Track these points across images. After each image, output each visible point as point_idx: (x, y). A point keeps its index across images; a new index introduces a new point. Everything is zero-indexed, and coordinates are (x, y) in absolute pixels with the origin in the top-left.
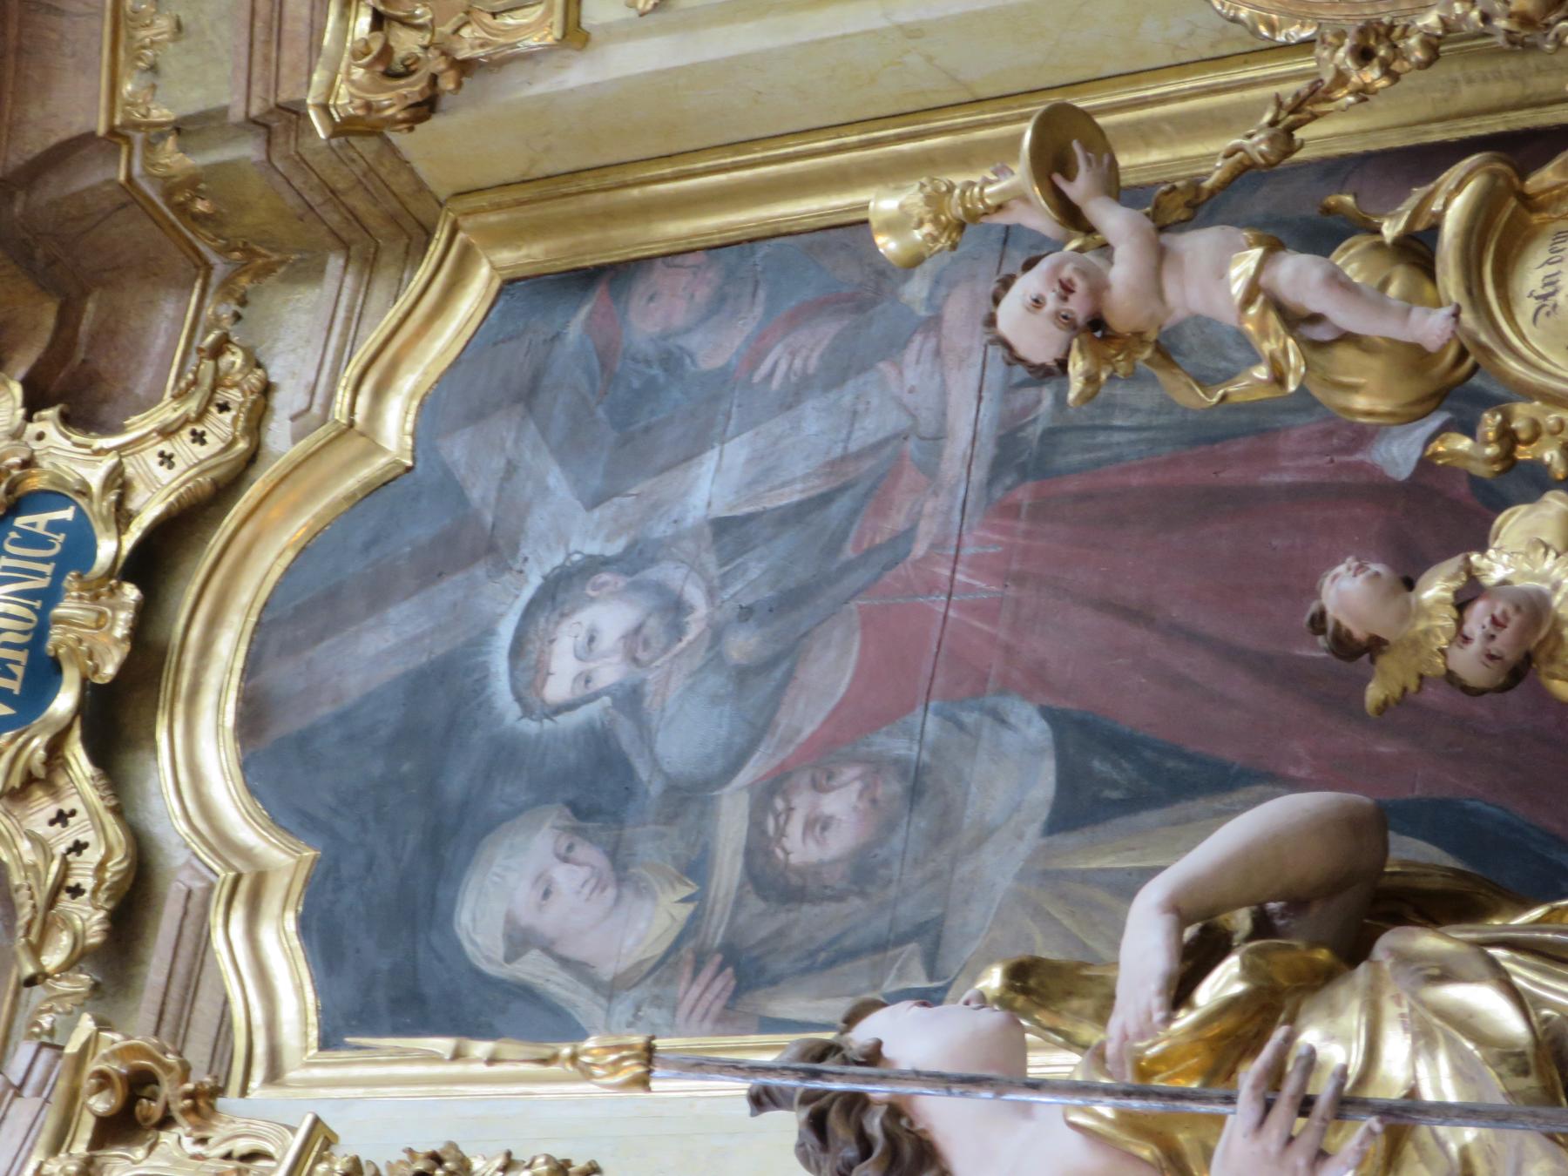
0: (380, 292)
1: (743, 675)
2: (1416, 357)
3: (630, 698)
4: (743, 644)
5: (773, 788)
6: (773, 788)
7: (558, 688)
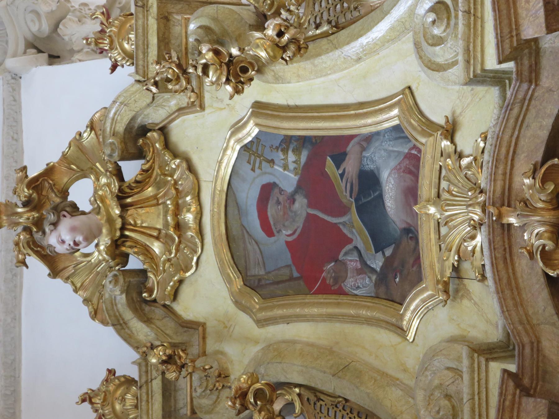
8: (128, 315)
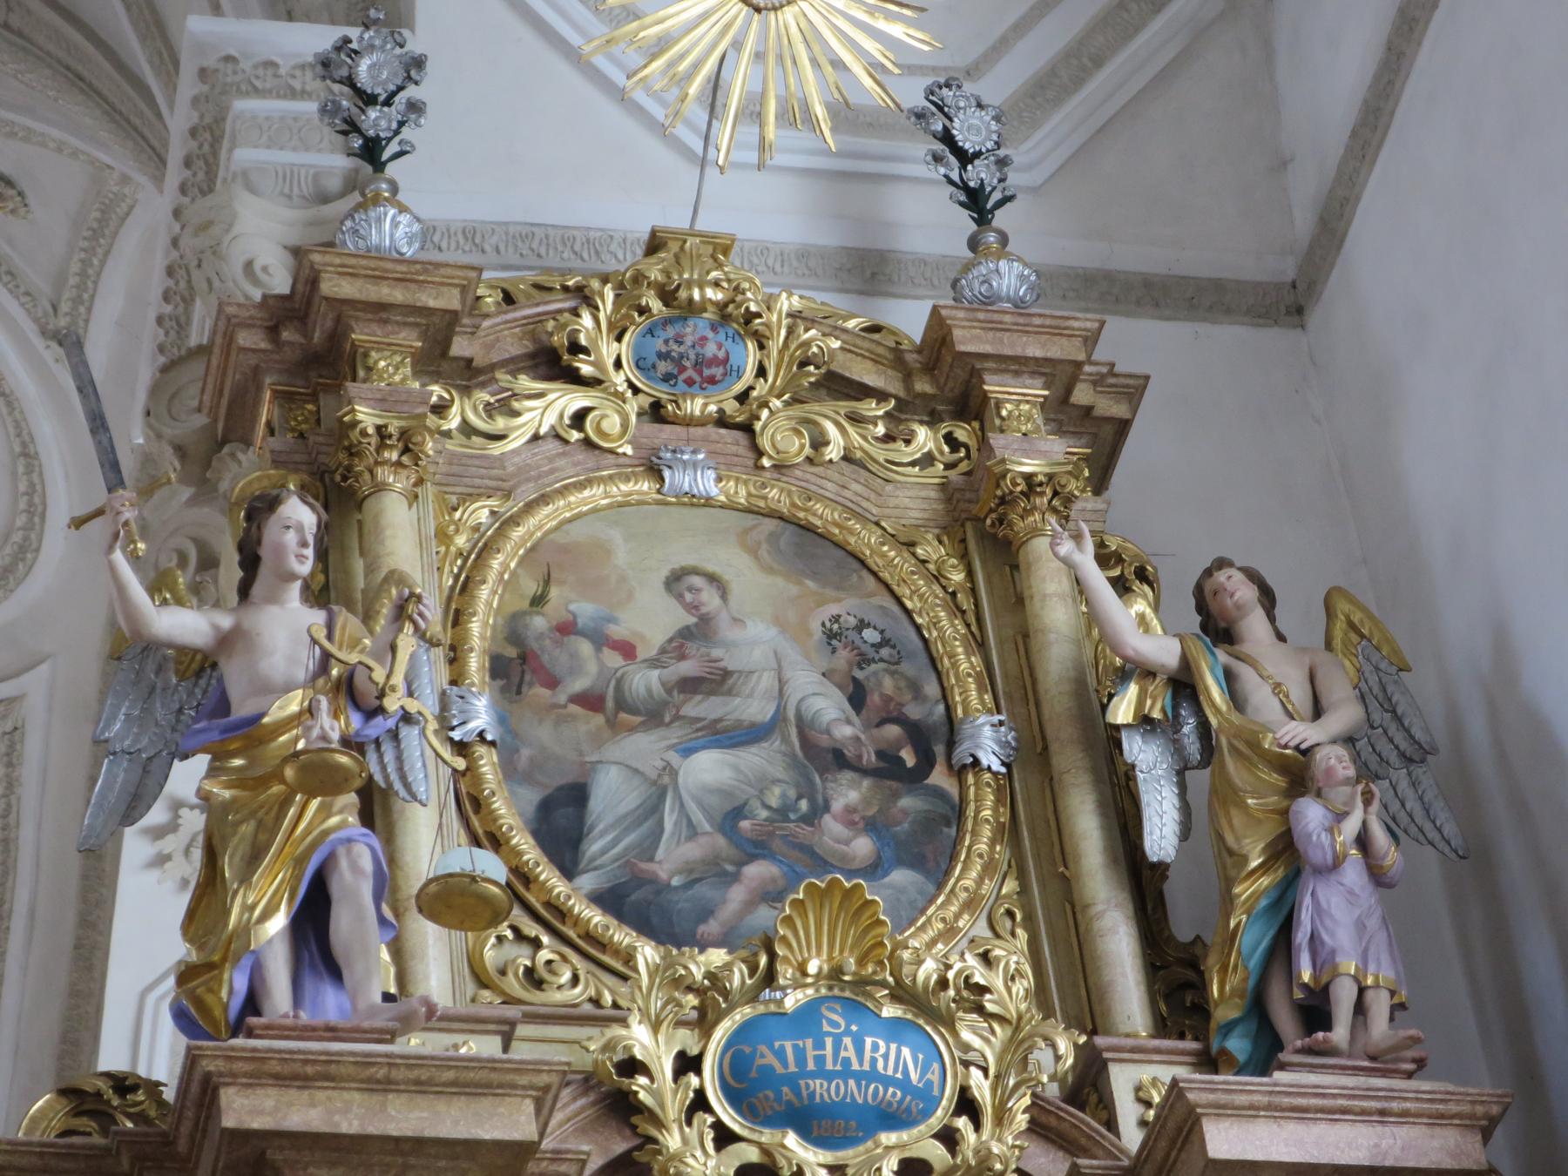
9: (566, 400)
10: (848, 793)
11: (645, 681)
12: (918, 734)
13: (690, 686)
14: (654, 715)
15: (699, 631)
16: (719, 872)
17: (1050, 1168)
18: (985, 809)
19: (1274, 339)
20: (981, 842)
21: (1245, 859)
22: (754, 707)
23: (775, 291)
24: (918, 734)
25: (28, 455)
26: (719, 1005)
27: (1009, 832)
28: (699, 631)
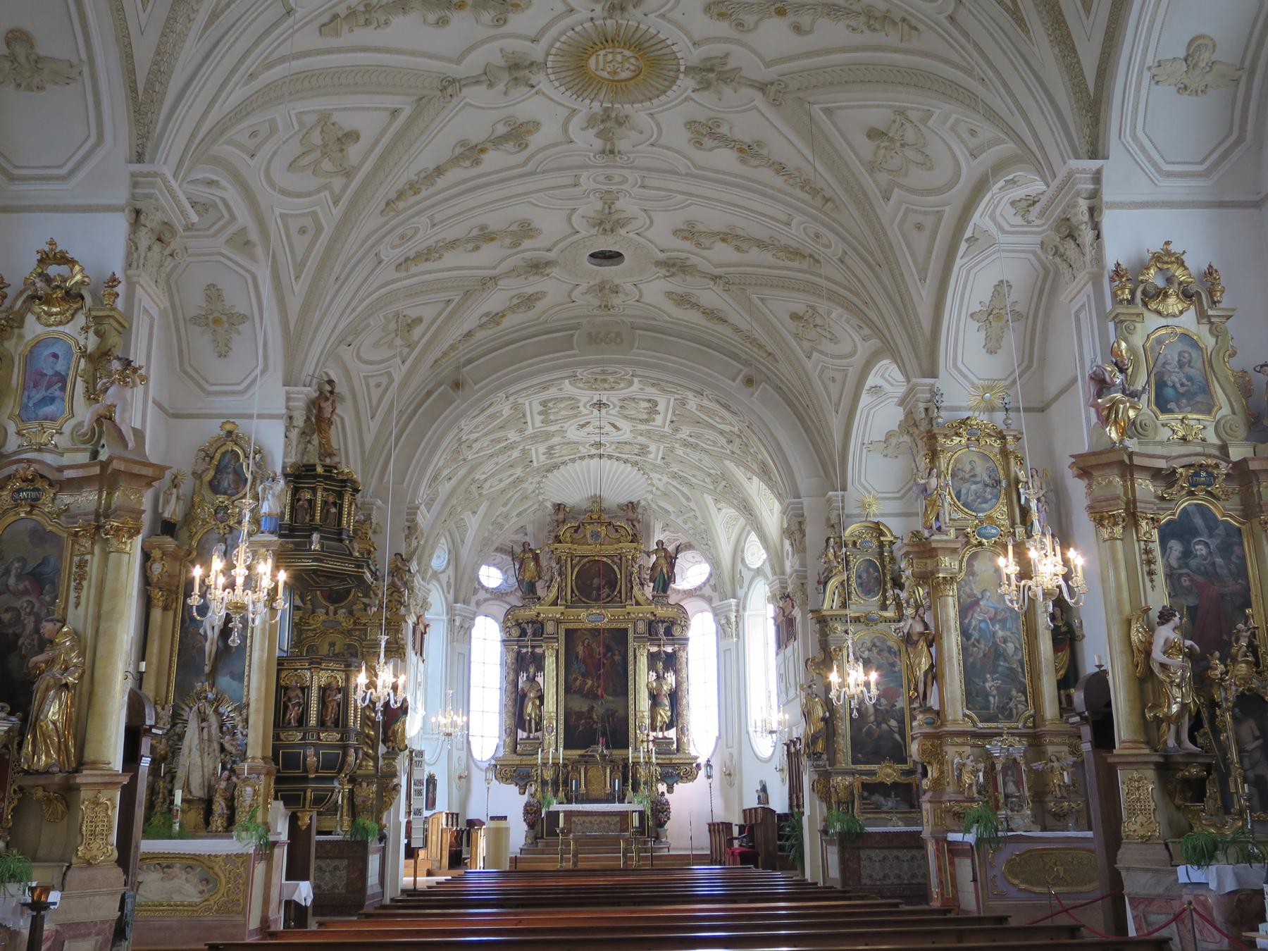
0: (1238, 513)
1: (1199, 569)
2: (1237, 655)
3: (1196, 556)
4: (1202, 568)
5: (1189, 575)
6: (1189, 575)
7: (1197, 547)
8: (25, 296)
9: (959, 439)
10: (988, 490)
11: (967, 476)
12: (996, 481)
13: (972, 476)
14: (968, 481)
15: (973, 469)
16: (974, 501)
17: (21, 267)
18: (1003, 492)
19: (1040, 415)
20: (1003, 496)
21: (31, 880)
22: (978, 479)
23: (1054, 184)
24: (996, 481)
25: (666, 4)
26: (387, 642)
27: (1006, 494)
28: (973, 469)
